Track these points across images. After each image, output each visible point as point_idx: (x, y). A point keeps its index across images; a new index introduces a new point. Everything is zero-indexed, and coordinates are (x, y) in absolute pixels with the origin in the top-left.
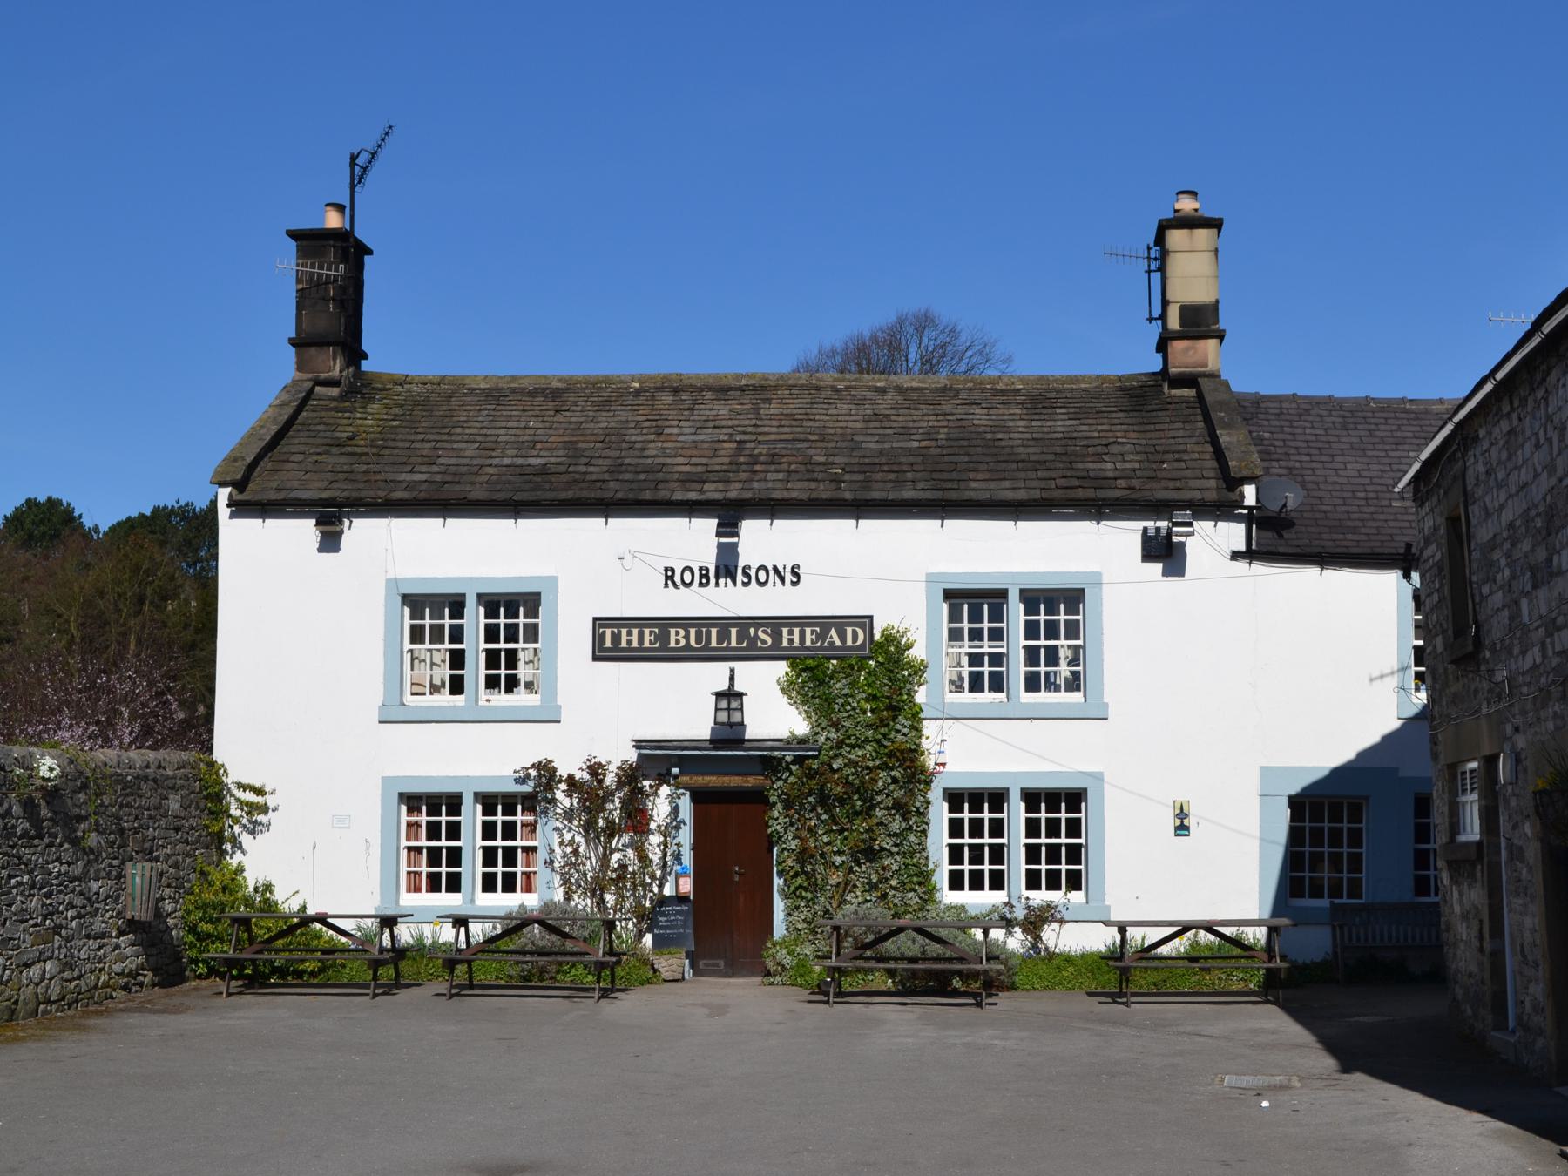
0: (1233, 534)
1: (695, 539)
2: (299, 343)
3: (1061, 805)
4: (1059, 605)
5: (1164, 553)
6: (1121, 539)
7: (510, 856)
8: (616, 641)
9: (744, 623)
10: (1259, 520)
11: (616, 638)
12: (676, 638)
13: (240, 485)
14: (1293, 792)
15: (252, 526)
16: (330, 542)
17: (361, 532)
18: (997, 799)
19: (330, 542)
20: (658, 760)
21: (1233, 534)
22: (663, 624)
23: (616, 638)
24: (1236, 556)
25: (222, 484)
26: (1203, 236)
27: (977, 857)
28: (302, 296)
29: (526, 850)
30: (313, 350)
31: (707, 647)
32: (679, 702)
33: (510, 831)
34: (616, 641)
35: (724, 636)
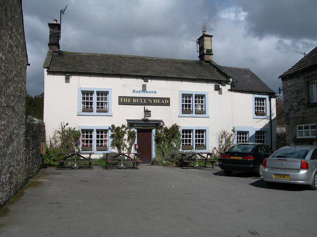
0: (228, 87)
1: (140, 82)
2: (49, 45)
3: (201, 132)
4: (201, 97)
5: (217, 89)
6: (211, 86)
7: (102, 142)
8: (124, 101)
9: (143, 98)
10: (232, 86)
11: (123, 100)
12: (134, 101)
13: (48, 68)
14: (258, 130)
15: (51, 77)
16: (67, 80)
17: (74, 79)
18: (91, 131)
19: (67, 80)
20: (131, 123)
21: (228, 87)
22: (132, 98)
23: (123, 100)
24: (229, 90)
25: (45, 68)
26: (209, 38)
27: (186, 142)
28: (50, 36)
29: (105, 140)
30: (53, 46)
31: (140, 103)
32: (136, 113)
33: (102, 137)
34: (124, 101)
35: (143, 101)
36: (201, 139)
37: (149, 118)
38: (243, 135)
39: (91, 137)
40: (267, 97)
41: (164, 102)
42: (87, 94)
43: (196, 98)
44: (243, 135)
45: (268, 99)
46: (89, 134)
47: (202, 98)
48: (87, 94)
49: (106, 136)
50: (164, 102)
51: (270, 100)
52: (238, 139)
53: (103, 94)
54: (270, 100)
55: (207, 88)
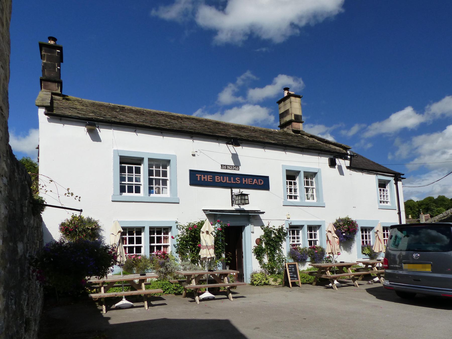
4: (310, 175)
6: (325, 160)
7: (159, 248)
8: (198, 178)
17: (105, 133)
18: (139, 231)
32: (221, 199)
33: (159, 240)
34: (198, 178)
36: (135, 245)
37: (246, 208)
38: (366, 233)
39: (139, 241)
40: (392, 179)
41: (262, 183)
42: (128, 164)
43: (150, 166)
44: (366, 233)
45: (393, 181)
46: (135, 236)
47: (165, 167)
48: (128, 164)
49: (166, 238)
50: (262, 183)
51: (396, 184)
52: (363, 238)
53: (160, 166)
54: (396, 184)
55: (318, 163)
